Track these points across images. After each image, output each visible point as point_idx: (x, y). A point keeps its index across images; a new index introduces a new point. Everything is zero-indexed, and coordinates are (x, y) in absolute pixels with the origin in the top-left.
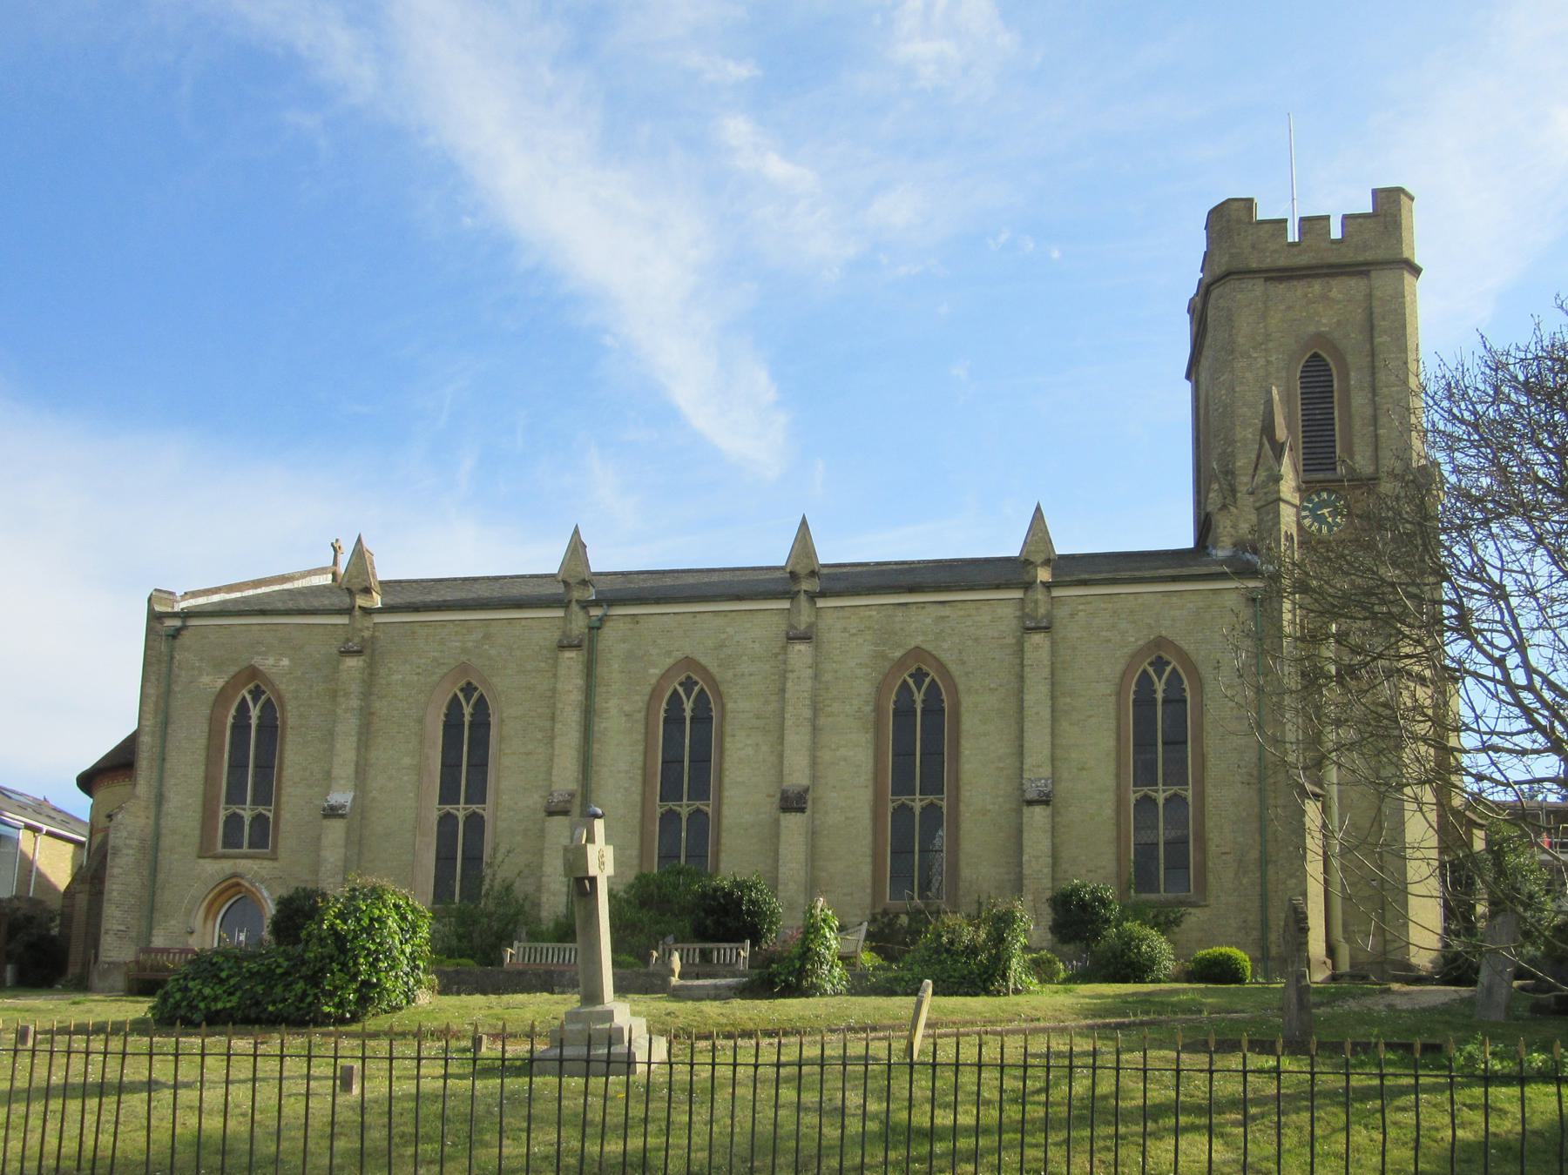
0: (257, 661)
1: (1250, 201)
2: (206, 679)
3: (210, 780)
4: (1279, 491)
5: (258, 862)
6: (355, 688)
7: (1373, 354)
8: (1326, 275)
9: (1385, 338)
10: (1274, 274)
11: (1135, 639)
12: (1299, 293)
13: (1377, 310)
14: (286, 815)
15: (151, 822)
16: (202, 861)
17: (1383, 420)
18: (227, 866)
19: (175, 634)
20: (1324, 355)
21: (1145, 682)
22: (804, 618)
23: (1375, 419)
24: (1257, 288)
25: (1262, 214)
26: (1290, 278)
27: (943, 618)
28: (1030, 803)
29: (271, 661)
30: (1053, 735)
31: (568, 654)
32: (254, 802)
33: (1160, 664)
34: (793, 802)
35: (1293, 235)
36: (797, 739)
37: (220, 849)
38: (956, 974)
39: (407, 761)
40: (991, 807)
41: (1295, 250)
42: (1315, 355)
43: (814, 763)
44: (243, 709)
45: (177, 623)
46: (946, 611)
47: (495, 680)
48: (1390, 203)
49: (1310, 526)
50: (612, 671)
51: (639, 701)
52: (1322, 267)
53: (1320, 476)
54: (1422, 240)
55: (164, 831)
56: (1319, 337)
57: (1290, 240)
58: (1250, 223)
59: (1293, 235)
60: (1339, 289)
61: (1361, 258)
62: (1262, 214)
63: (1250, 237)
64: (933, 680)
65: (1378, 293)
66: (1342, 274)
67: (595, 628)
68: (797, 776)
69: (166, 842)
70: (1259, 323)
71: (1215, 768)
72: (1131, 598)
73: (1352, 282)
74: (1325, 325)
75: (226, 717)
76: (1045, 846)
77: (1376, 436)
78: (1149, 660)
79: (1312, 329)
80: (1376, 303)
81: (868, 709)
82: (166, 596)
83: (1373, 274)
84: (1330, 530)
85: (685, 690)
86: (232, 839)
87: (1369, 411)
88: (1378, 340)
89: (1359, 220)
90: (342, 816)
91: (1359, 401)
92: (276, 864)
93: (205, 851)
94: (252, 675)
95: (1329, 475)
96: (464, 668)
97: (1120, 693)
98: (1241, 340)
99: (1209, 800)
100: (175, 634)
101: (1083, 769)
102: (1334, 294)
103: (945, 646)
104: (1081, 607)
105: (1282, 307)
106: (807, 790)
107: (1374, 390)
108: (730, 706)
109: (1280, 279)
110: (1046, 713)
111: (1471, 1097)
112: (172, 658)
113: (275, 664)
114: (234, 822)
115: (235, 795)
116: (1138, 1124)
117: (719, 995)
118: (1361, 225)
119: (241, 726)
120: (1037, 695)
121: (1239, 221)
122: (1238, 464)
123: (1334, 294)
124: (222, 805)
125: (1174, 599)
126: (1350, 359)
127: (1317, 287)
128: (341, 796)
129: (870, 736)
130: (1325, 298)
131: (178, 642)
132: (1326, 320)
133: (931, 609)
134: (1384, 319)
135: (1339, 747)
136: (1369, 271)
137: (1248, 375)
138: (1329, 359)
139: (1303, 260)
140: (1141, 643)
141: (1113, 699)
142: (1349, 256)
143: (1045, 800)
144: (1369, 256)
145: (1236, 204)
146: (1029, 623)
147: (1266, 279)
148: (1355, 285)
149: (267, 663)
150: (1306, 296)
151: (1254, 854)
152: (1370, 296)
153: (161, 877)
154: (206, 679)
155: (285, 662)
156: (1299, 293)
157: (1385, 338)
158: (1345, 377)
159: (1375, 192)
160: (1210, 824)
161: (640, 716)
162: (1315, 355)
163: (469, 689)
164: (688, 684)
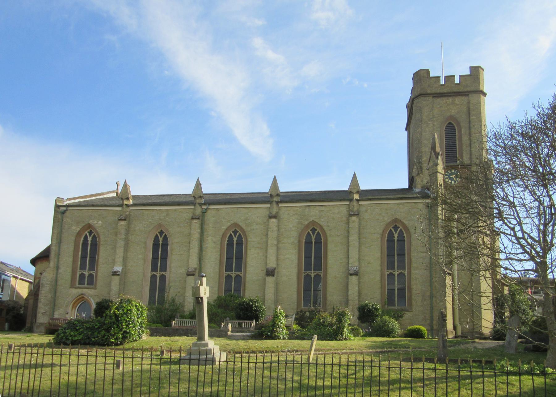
0: (91, 222)
1: (428, 70)
2: (74, 228)
3: (74, 262)
4: (437, 169)
5: (90, 290)
6: (123, 232)
7: (470, 122)
8: (454, 96)
9: (474, 117)
11: (388, 219)
12: (444, 101)
13: (471, 108)
14: (100, 274)
15: (55, 275)
16: (71, 289)
17: (473, 145)
18: (79, 291)
19: (64, 213)
20: (453, 123)
21: (391, 234)
22: (275, 210)
23: (470, 145)
24: (430, 99)
25: (432, 74)
26: (442, 96)
27: (322, 211)
28: (351, 275)
29: (95, 222)
30: (359, 251)
31: (195, 221)
32: (89, 269)
33: (396, 228)
34: (270, 273)
35: (442, 82)
36: (272, 251)
37: (77, 285)
39: (140, 256)
40: (337, 276)
41: (443, 87)
42: (450, 123)
43: (278, 259)
44: (86, 238)
45: (64, 209)
46: (323, 208)
47: (170, 229)
48: (476, 71)
49: (448, 181)
50: (209, 227)
51: (219, 237)
52: (452, 93)
53: (452, 164)
54: (487, 84)
55: (59, 279)
56: (451, 117)
57: (441, 83)
58: (428, 77)
59: (442, 82)
60: (458, 100)
61: (465, 90)
62: (432, 74)
64: (240, 234)
65: (471, 102)
67: (204, 212)
68: (272, 264)
69: (60, 282)
71: (414, 264)
72: (386, 205)
73: (463, 98)
75: (80, 241)
76: (356, 289)
77: (471, 151)
78: (392, 226)
79: (449, 114)
80: (471, 105)
81: (296, 241)
82: (61, 199)
83: (470, 95)
85: (312, 233)
86: (81, 282)
87: (468, 142)
88: (471, 118)
89: (465, 77)
90: (118, 275)
91: (465, 139)
92: (96, 291)
93: (72, 286)
94: (89, 228)
95: (455, 164)
96: (160, 225)
97: (382, 238)
98: (424, 117)
99: (412, 275)
100: (64, 213)
101: (369, 263)
102: (456, 102)
103: (323, 220)
104: (369, 208)
105: (439, 106)
106: (275, 269)
107: (470, 128)
108: (249, 240)
110: (357, 244)
112: (63, 220)
113: (97, 223)
114: (82, 276)
115: (83, 267)
116: (387, 386)
118: (466, 79)
119: (85, 244)
120: (354, 237)
121: (424, 77)
122: (423, 160)
123: (456, 102)
124: (78, 270)
125: (401, 206)
126: (462, 124)
127: (450, 100)
128: (118, 268)
129: (297, 251)
131: (65, 215)
132: (453, 111)
133: (318, 208)
136: (469, 94)
137: (427, 129)
138: (455, 124)
139: (446, 90)
140: (390, 220)
141: (380, 239)
142: (462, 89)
143: (356, 274)
144: (469, 89)
145: (423, 71)
146: (351, 213)
147: (433, 97)
148: (464, 99)
149: (94, 223)
151: (428, 294)
152: (469, 103)
153: (58, 294)
154: (74, 228)
155: (100, 222)
157: (474, 117)
158: (460, 131)
159: (471, 68)
160: (413, 283)
161: (219, 243)
162: (450, 123)
163: (161, 232)
164: (235, 232)
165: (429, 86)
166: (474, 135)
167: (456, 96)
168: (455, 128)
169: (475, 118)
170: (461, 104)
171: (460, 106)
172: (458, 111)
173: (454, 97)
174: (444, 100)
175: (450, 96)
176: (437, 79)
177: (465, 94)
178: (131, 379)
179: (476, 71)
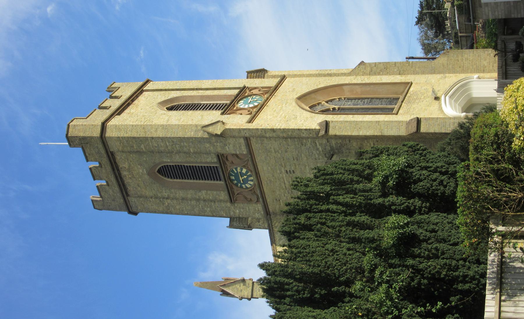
8: (118, 170)
10: (124, 192)
12: (130, 181)
26: (124, 185)
38: (422, 97)
48: (246, 72)
63: (110, 201)
66: (115, 162)
70: (150, 201)
74: (143, 171)
79: (146, 177)
84: (250, 176)
89: (87, 155)
105: (139, 188)
109: (126, 189)
111: (514, 254)
117: (371, 72)
118: (89, 154)
127: (124, 173)
130: (129, 170)
132: (140, 170)
134: (133, 147)
135: (301, 168)
136: (111, 152)
147: (128, 195)
150: (131, 178)
156: (130, 181)
165: (114, 200)
166: (169, 148)
167: (117, 167)
168: (160, 168)
169: (142, 145)
170: (128, 160)
171: (131, 161)
172: (139, 165)
173: (120, 169)
174: (127, 180)
175: (120, 174)
176: (101, 190)
177: (111, 157)
178: (502, 309)
179: (246, 72)
